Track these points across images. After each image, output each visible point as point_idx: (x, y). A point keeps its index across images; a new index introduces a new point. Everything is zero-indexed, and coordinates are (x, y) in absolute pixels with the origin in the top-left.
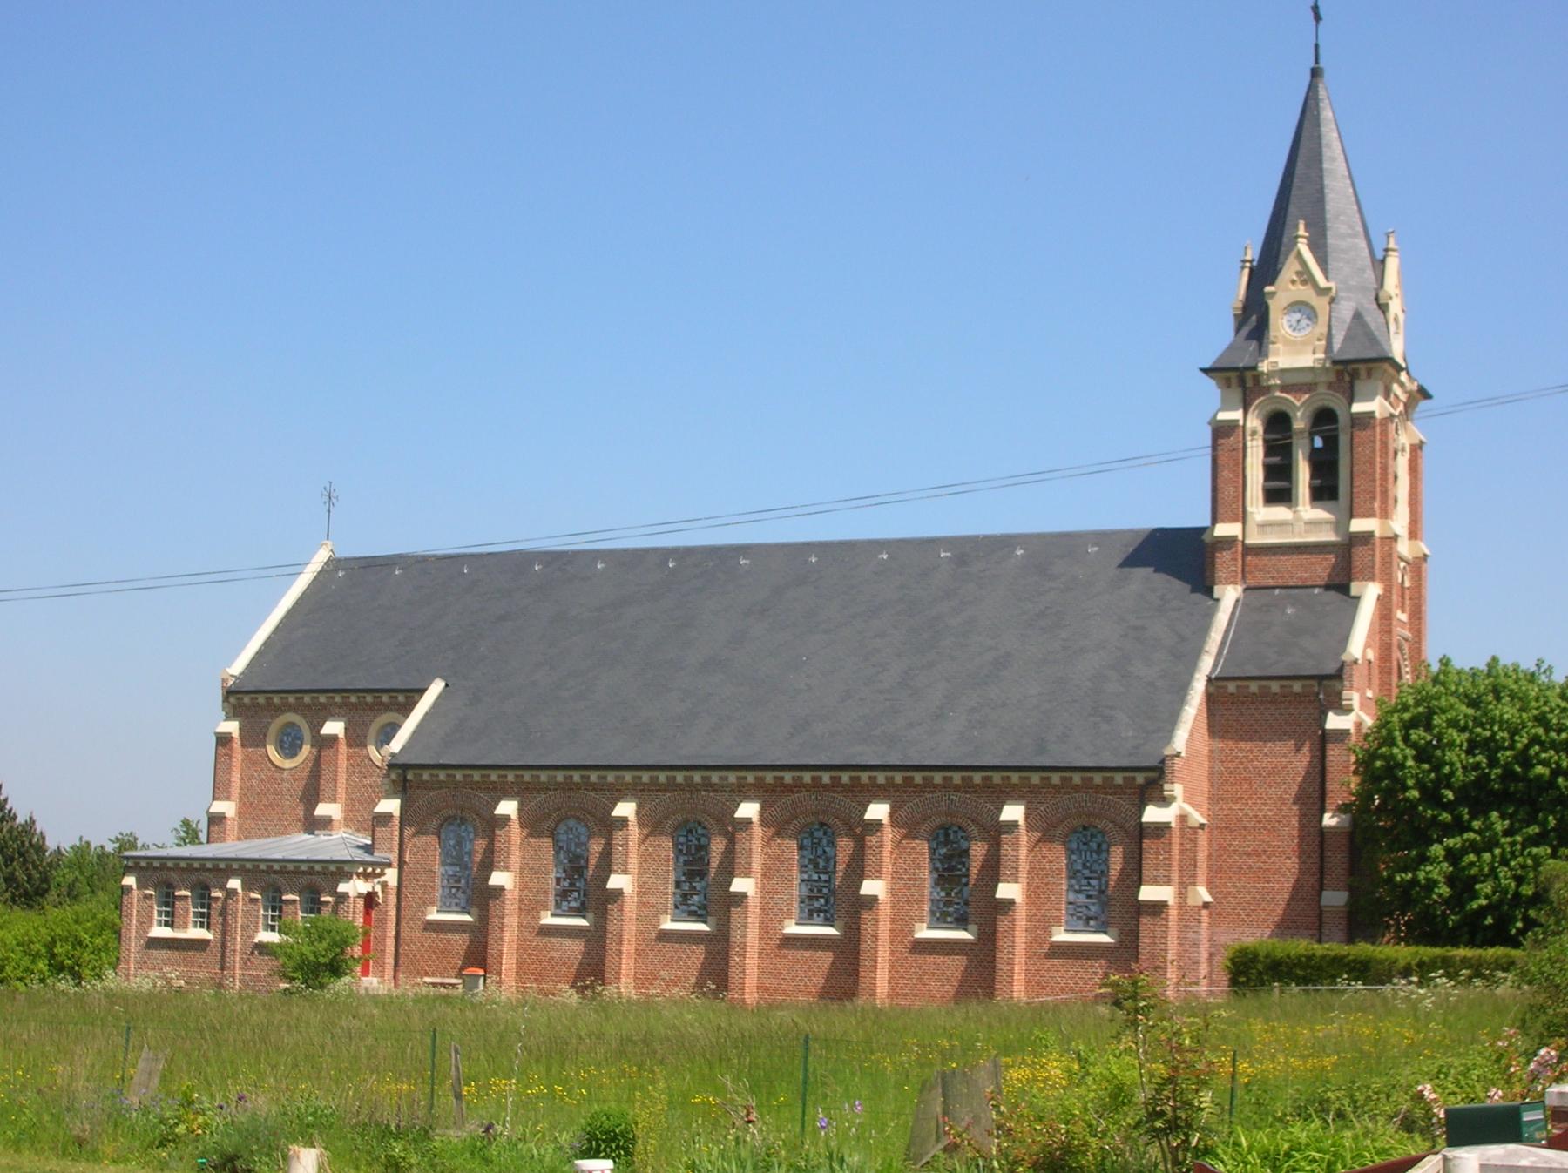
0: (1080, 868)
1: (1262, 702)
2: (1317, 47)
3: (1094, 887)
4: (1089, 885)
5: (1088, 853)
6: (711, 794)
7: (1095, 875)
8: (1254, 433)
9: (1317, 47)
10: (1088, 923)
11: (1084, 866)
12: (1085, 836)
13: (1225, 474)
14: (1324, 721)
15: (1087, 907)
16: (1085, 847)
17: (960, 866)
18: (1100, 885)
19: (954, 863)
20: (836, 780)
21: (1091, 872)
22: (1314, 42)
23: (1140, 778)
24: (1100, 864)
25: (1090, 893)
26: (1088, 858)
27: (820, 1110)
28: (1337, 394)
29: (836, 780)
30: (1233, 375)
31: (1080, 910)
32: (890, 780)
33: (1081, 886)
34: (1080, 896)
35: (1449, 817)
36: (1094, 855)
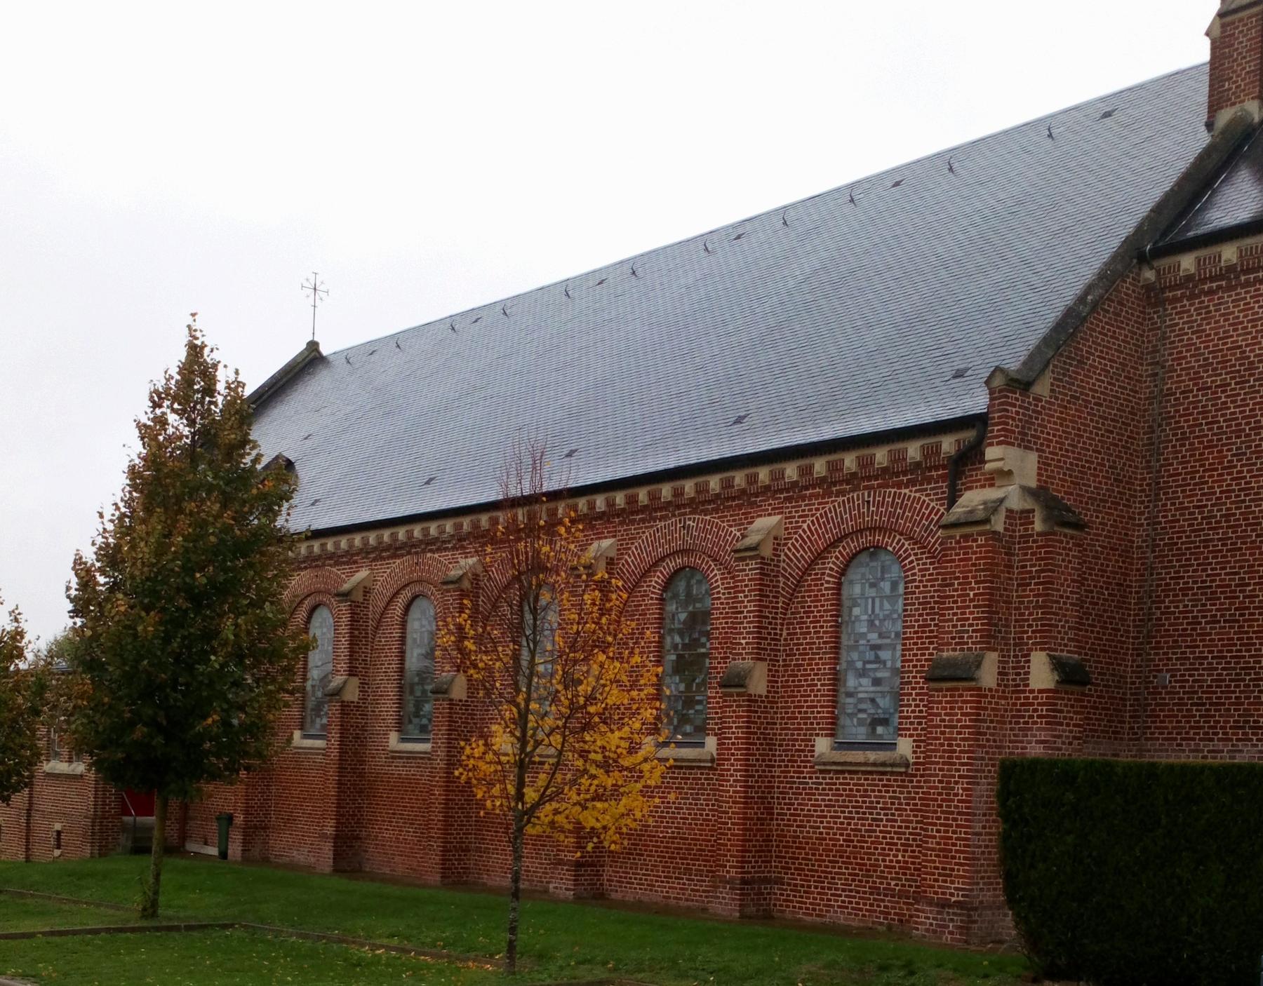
0: (864, 630)
1: (1247, 284)
4: (877, 660)
5: (877, 601)
6: (436, 555)
7: (888, 641)
10: (874, 730)
11: (871, 623)
15: (873, 700)
16: (872, 592)
18: (894, 661)
21: (881, 636)
23: (948, 444)
24: (894, 621)
25: (879, 675)
34: (865, 681)
36: (887, 606)
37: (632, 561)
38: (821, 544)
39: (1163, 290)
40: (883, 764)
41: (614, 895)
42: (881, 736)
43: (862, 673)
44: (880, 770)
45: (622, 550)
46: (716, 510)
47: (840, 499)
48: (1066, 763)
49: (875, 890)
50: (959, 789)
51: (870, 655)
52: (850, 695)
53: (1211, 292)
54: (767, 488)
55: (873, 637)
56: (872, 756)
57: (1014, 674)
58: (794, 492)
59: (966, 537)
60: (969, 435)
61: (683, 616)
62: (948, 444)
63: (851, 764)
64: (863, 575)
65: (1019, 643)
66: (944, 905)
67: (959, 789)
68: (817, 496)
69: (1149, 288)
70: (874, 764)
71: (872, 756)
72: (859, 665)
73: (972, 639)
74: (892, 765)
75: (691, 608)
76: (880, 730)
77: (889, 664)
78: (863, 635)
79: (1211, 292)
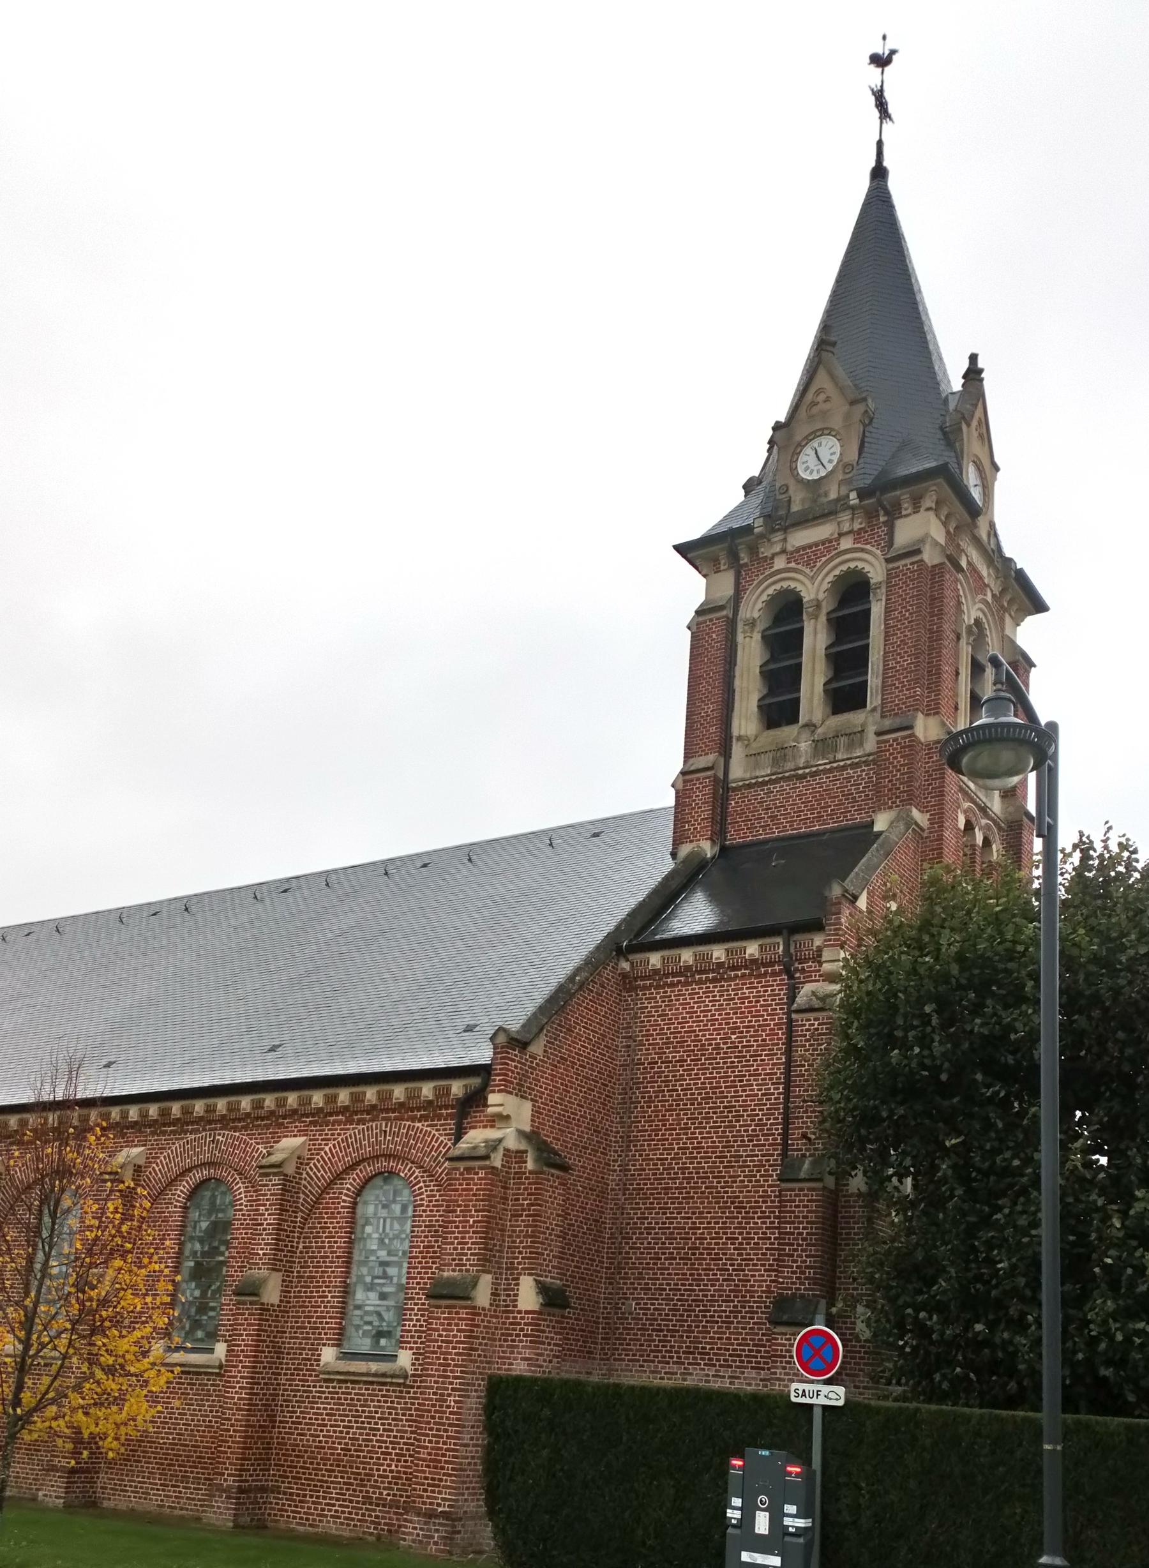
0: (374, 1247)
1: (700, 982)
2: (880, 144)
3: (391, 1278)
4: (385, 1276)
8: (752, 624)
9: (880, 144)
10: (378, 1342)
11: (381, 1241)
12: (385, 1193)
13: (711, 709)
14: (1108, 1160)
16: (383, 1213)
17: (223, 1248)
18: (400, 1277)
19: (216, 1244)
20: (412, 1095)
21: (389, 1254)
22: (877, 138)
23: (457, 1088)
25: (387, 1289)
26: (388, 1230)
27: (1132, 879)
28: (868, 547)
29: (385, 1097)
30: (720, 550)
31: (367, 1318)
32: (412, 1095)
33: (374, 1277)
35: (1093, 1238)
36: (396, 1226)
37: (160, 1169)
38: (341, 1166)
39: (636, 979)
40: (384, 1375)
41: (105, 1504)
42: (383, 1349)
43: (370, 1288)
44: (381, 1379)
45: (151, 1159)
46: (245, 1128)
47: (361, 1127)
48: (546, 1380)
49: (368, 1500)
50: (451, 1401)
51: (378, 1271)
52: (358, 1307)
53: (672, 985)
54: (295, 1112)
55: (383, 1254)
56: (374, 1367)
57: (505, 1295)
58: (320, 1117)
59: (468, 1170)
60: (475, 1082)
61: (204, 1225)
62: (457, 1088)
63: (354, 1374)
64: (377, 1196)
65: (511, 1268)
66: (431, 1515)
67: (451, 1401)
68: (339, 1123)
69: (624, 976)
70: (375, 1375)
71: (374, 1367)
72: (368, 1279)
73: (470, 1261)
74: (393, 1376)
75: (213, 1218)
76: (383, 1342)
77: (395, 1280)
78: (373, 1252)
79: (672, 985)
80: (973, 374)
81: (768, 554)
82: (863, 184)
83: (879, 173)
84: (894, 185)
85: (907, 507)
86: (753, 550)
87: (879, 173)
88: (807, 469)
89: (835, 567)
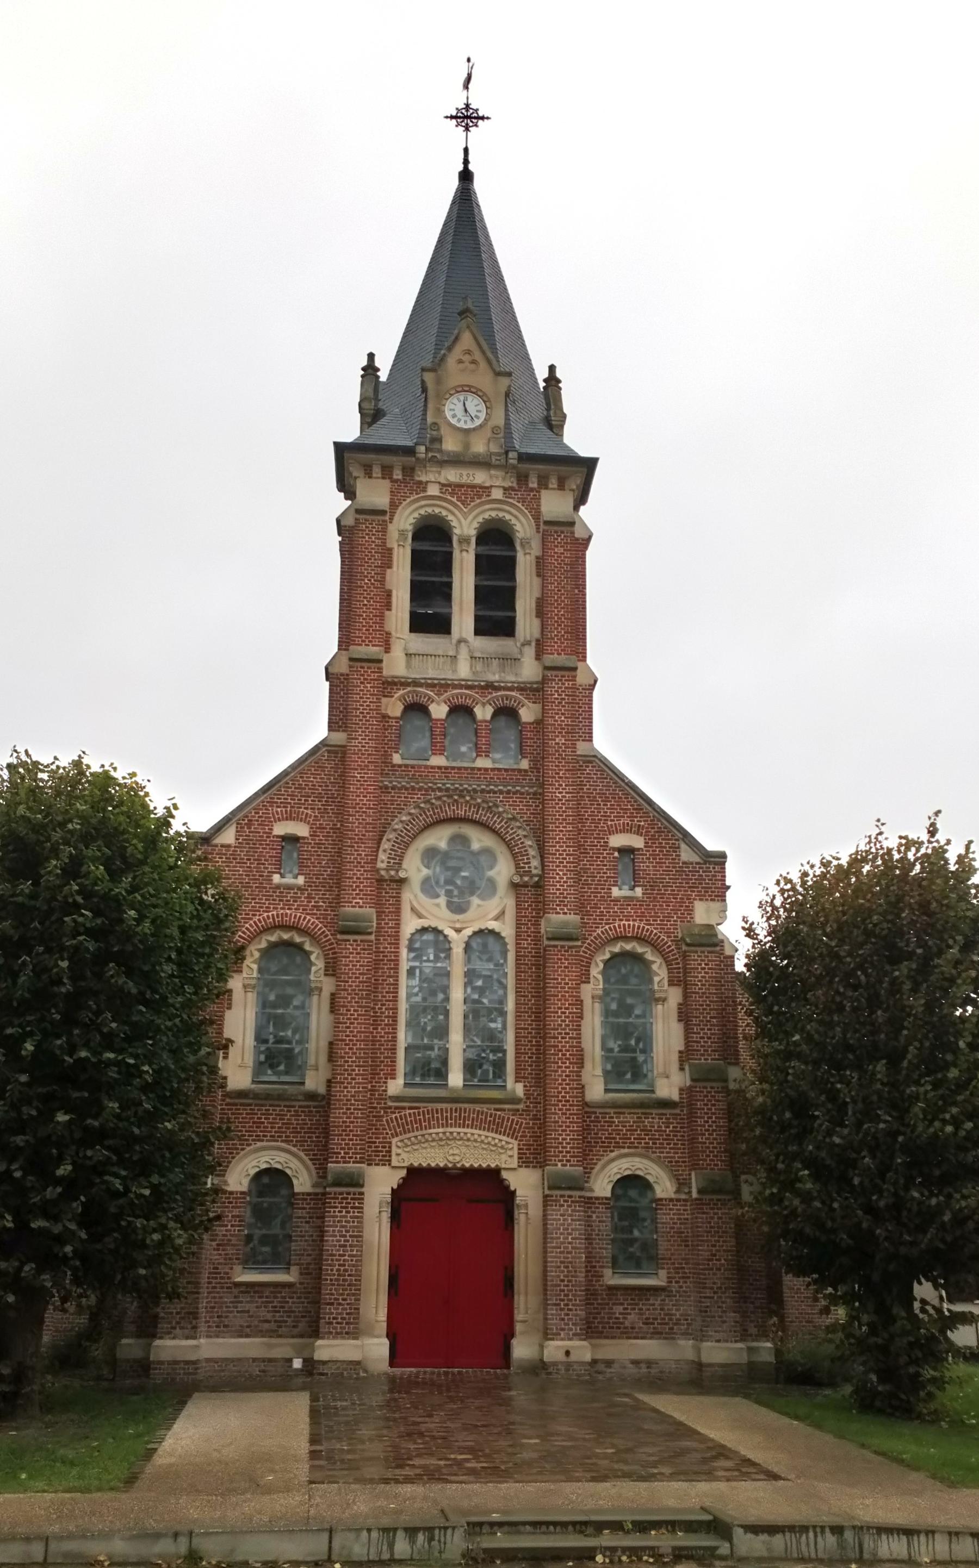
2: (466, 150)
9: (466, 150)
80: (553, 380)
81: (423, 478)
82: (455, 183)
83: (466, 176)
84: (479, 185)
85: (553, 483)
86: (409, 471)
87: (466, 176)
88: (454, 416)
89: (422, 507)
